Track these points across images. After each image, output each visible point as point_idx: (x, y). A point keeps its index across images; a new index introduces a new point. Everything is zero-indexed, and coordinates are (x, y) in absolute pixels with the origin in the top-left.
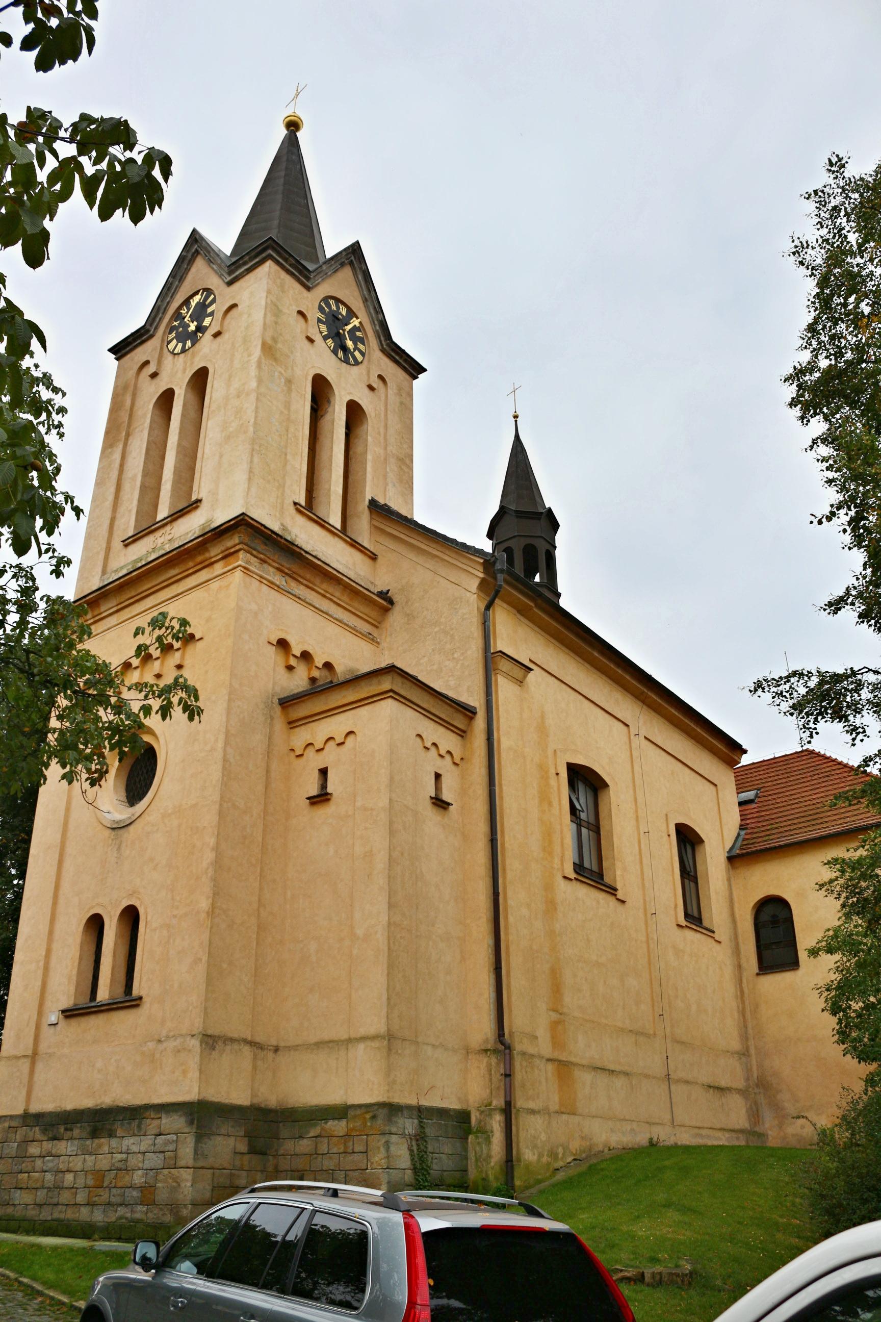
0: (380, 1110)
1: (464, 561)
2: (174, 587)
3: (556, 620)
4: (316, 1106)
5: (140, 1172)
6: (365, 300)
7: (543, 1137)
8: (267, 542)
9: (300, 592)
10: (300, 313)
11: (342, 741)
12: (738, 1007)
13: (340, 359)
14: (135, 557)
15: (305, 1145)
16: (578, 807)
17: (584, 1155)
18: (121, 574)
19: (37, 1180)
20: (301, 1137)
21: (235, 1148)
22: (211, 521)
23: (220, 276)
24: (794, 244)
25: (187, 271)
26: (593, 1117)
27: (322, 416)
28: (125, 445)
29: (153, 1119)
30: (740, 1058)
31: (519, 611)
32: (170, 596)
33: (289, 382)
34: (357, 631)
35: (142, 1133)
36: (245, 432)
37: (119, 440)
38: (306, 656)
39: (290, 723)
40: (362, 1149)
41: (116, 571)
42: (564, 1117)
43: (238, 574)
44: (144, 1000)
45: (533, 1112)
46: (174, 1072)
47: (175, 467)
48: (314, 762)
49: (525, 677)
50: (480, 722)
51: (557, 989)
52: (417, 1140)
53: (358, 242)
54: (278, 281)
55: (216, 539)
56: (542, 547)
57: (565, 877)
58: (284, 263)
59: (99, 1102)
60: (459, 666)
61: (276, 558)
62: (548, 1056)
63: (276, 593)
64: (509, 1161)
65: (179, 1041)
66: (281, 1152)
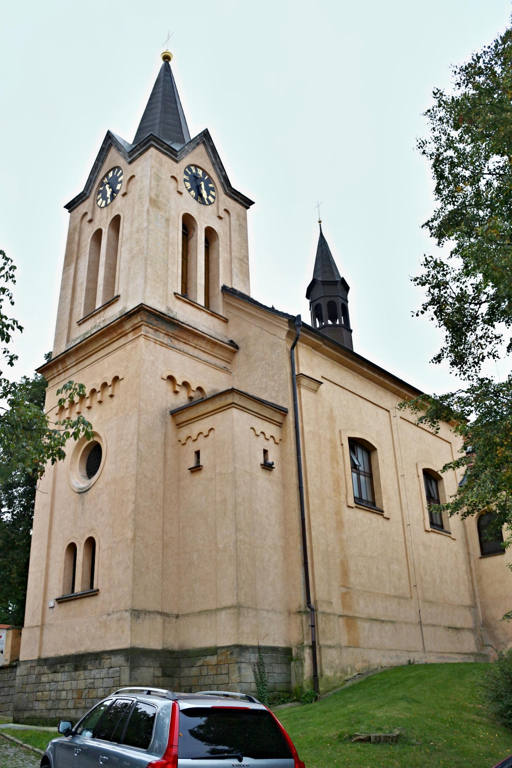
0: (235, 649)
1: (278, 320)
2: (106, 349)
3: (338, 351)
4: (200, 648)
5: (101, 689)
6: (213, 164)
7: (337, 662)
8: (158, 319)
9: (180, 347)
10: (173, 177)
11: (207, 434)
12: (468, 578)
13: (200, 202)
14: (84, 332)
15: (194, 671)
16: (357, 463)
17: (365, 672)
18: (77, 342)
19: (47, 696)
20: (192, 666)
21: (154, 674)
22: (125, 308)
23: (125, 158)
24: (418, 143)
25: (106, 156)
26: (371, 648)
27: (190, 238)
28: (77, 264)
29: (107, 659)
30: (470, 610)
31: (313, 348)
32: (104, 354)
33: (167, 220)
34: (217, 367)
35: (101, 667)
36: (142, 254)
37: (73, 262)
38: (186, 384)
39: (177, 425)
40: (226, 672)
41: (74, 340)
42: (351, 650)
43: (142, 339)
44: (100, 591)
45: (330, 647)
46: (117, 632)
47: (105, 276)
48: (192, 447)
49: (318, 388)
50: (290, 417)
51: (345, 573)
52: (258, 666)
53: (207, 129)
54: (158, 160)
55: (127, 319)
56: (340, 301)
57: (349, 507)
58: (160, 148)
59: (78, 650)
60: (277, 384)
61: (164, 327)
62: (340, 614)
63: (165, 349)
64: (315, 677)
65: (119, 614)
66: (182, 675)
